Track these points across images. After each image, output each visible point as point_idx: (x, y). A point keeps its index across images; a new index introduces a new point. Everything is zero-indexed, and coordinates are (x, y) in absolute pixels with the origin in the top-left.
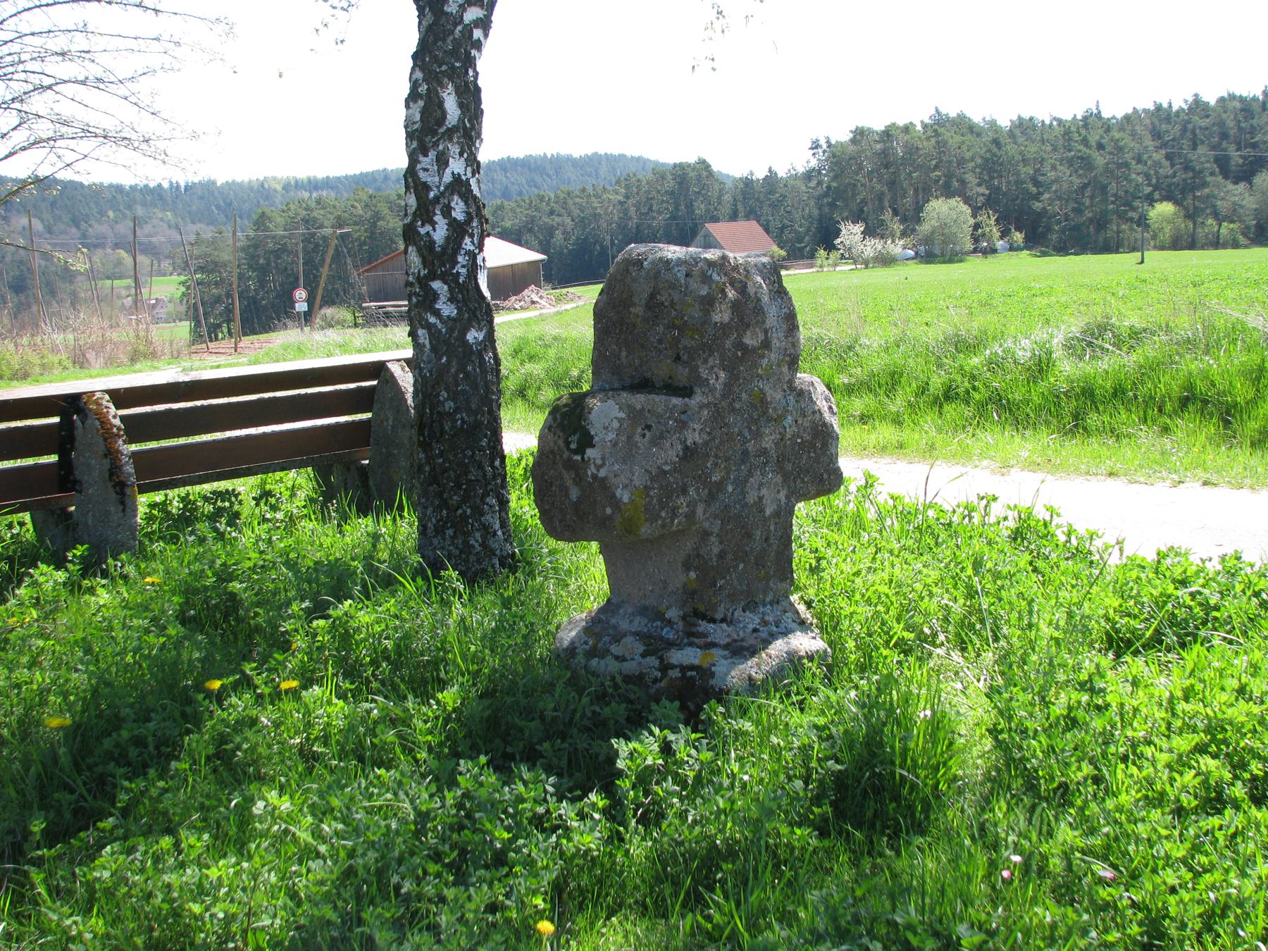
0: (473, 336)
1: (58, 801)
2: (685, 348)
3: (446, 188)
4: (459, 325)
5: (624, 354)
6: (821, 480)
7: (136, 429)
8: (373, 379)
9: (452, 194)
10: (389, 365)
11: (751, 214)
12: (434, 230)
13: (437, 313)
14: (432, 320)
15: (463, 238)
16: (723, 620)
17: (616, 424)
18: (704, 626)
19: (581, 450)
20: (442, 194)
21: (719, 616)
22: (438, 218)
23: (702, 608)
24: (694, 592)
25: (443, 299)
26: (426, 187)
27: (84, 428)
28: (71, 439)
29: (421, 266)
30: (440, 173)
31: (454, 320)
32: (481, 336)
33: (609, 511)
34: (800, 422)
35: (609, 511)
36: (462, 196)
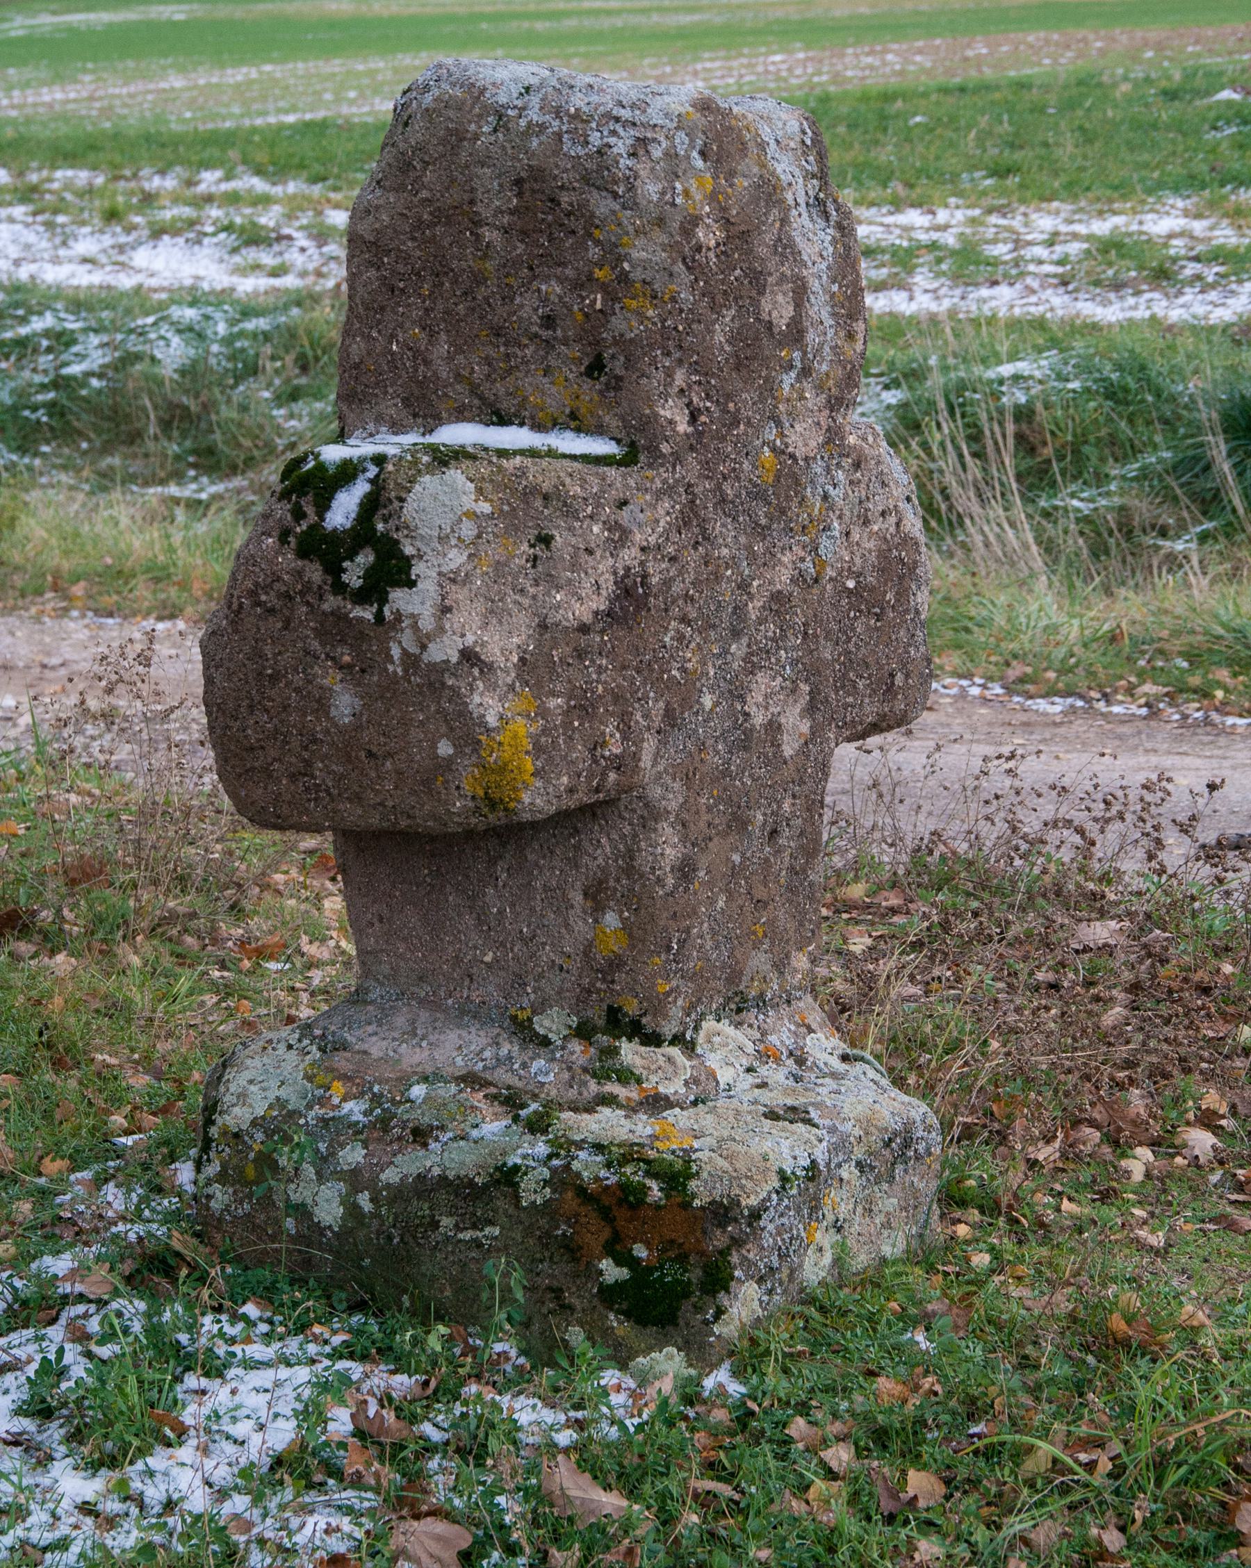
1: (691, 1365)
2: (619, 341)
6: (890, 688)
16: (677, 1040)
17: (468, 530)
18: (630, 1053)
19: (375, 589)
23: (632, 1008)
24: (616, 963)
33: (445, 749)
34: (855, 536)
35: (445, 749)
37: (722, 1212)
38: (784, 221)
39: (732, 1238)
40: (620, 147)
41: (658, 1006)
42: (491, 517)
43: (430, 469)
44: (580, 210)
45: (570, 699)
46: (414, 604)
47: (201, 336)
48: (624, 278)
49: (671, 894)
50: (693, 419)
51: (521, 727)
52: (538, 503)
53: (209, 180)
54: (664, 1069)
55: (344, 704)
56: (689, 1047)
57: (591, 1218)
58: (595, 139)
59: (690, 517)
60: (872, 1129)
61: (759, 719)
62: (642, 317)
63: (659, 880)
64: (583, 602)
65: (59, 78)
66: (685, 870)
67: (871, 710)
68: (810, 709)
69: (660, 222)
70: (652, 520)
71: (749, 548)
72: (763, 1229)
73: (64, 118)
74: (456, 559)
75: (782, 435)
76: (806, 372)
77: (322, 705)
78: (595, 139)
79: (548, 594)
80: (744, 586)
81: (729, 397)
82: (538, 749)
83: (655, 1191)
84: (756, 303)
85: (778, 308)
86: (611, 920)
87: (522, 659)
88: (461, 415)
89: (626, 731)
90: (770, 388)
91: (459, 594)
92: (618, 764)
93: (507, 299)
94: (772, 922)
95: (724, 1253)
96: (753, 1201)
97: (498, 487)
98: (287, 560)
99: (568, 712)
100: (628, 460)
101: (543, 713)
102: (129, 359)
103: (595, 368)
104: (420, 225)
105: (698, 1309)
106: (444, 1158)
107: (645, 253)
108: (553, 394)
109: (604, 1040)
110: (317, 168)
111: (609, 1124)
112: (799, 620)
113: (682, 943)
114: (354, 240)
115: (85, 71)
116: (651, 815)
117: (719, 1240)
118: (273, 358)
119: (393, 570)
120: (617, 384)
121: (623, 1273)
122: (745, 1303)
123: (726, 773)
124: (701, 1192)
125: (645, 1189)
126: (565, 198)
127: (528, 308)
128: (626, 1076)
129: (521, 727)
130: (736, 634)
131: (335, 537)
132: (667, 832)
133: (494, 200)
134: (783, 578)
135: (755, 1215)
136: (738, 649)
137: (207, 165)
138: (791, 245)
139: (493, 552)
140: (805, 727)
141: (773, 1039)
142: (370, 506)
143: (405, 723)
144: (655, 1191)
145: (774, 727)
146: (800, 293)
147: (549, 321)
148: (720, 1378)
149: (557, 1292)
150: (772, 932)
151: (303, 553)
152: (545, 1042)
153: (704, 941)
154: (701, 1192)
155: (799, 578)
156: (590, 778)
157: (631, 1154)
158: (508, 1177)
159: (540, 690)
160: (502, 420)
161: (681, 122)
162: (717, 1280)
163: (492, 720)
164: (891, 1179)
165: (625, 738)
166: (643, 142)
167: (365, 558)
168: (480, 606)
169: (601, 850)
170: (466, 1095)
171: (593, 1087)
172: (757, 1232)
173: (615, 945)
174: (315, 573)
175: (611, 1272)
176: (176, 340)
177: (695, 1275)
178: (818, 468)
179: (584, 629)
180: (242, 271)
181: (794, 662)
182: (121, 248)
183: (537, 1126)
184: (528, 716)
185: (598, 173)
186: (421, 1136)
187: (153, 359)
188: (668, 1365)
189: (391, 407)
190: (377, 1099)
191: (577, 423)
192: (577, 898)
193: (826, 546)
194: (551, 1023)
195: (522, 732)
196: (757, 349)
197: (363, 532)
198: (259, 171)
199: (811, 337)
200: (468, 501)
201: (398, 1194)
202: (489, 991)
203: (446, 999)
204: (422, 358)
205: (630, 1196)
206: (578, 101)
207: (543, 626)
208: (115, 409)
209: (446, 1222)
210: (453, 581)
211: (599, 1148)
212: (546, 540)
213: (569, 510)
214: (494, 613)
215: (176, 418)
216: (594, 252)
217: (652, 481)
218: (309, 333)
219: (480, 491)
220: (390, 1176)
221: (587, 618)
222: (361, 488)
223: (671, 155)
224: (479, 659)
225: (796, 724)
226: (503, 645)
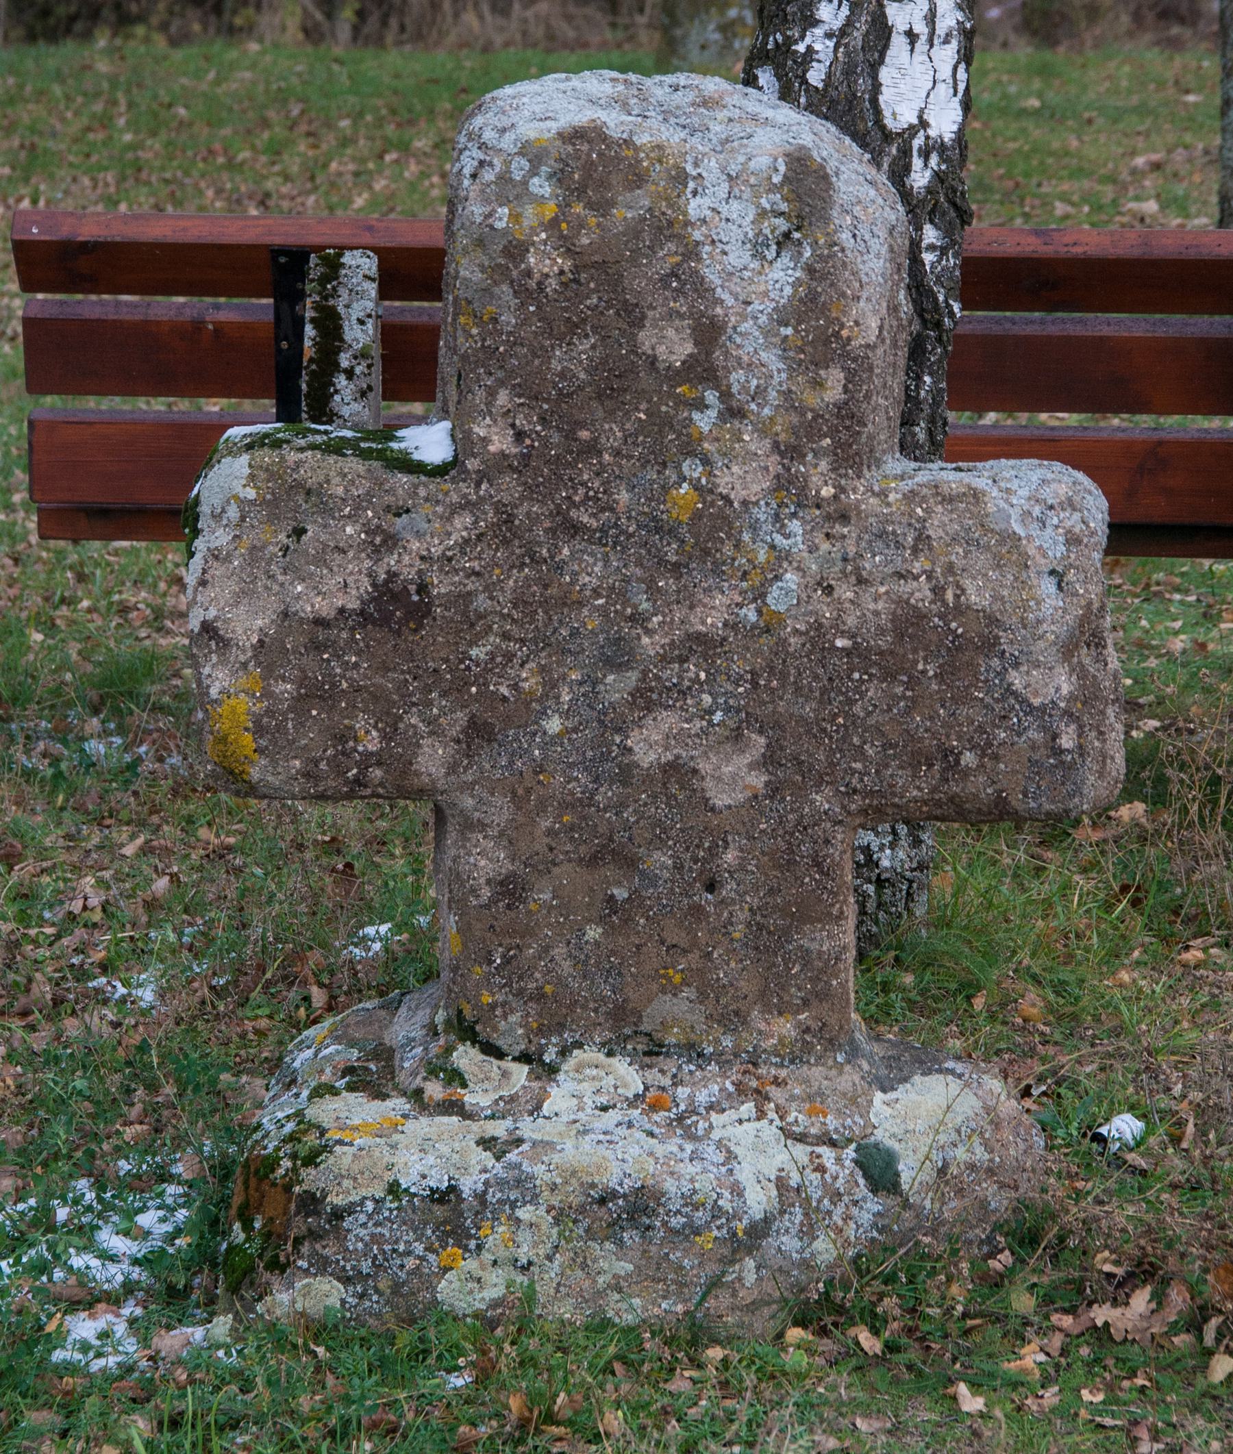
16: (524, 1058)
17: (233, 513)
39: (309, 1230)
42: (252, 503)
45: (300, 687)
49: (487, 906)
50: (519, 436)
51: (243, 705)
52: (300, 499)
60: (574, 1181)
63: (473, 891)
64: (337, 589)
68: (769, 761)
72: (349, 1231)
75: (710, 474)
79: (291, 583)
81: (582, 425)
87: (260, 641)
91: (218, 570)
101: (267, 694)
113: (507, 961)
128: (456, 1077)
135: (338, 1214)
136: (617, 686)
140: (758, 780)
146: (709, 332)
159: (269, 672)
172: (341, 1236)
178: (761, 514)
179: (320, 622)
184: (254, 695)
195: (242, 709)
207: (285, 614)
210: (216, 558)
212: (299, 532)
217: (446, 494)
219: (252, 477)
223: (504, 179)
224: (216, 633)
226: (248, 625)
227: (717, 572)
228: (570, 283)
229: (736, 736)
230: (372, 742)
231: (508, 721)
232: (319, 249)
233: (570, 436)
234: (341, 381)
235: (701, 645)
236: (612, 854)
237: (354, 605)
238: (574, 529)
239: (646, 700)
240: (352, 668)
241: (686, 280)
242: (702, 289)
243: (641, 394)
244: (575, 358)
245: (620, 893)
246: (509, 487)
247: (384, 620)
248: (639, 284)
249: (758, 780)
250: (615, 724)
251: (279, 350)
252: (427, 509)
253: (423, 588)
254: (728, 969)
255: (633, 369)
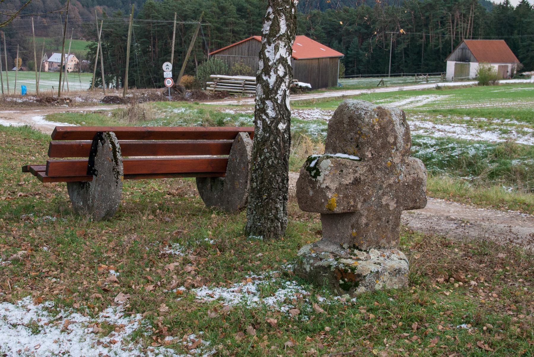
0: (282, 126)
2: (361, 142)
3: (277, 61)
4: (276, 121)
5: (338, 142)
7: (126, 150)
8: (232, 139)
9: (279, 64)
10: (241, 134)
11: (499, 35)
12: (270, 78)
13: (267, 115)
14: (264, 117)
15: (281, 83)
16: (365, 251)
17: (329, 168)
18: (356, 251)
19: (315, 177)
20: (275, 63)
21: (363, 249)
22: (272, 73)
23: (357, 245)
24: (355, 238)
25: (270, 109)
26: (268, 60)
27: (103, 147)
28: (96, 151)
29: (262, 93)
30: (275, 54)
31: (274, 118)
32: (284, 126)
33: (323, 201)
35: (323, 201)
36: (283, 65)
37: (359, 275)
38: (394, 126)
40: (363, 113)
41: (361, 245)
43: (325, 159)
44: (357, 123)
46: (320, 178)
47: (478, 149)
48: (362, 133)
50: (372, 155)
51: (335, 198)
53: (507, 121)
54: (362, 255)
55: (311, 193)
56: (368, 253)
57: (340, 274)
58: (360, 112)
59: (370, 170)
61: (384, 203)
62: (364, 139)
64: (348, 180)
65: (513, 100)
66: (367, 225)
67: (411, 205)
68: (397, 203)
69: (368, 125)
70: (362, 170)
71: (384, 176)
73: (510, 108)
74: (327, 172)
76: (397, 150)
77: (308, 193)
78: (360, 112)
80: (383, 182)
81: (380, 152)
82: (337, 202)
83: (350, 271)
84: (386, 139)
85: (391, 140)
86: (354, 231)
88: (340, 152)
89: (355, 201)
90: (389, 152)
91: (327, 178)
92: (353, 206)
93: (346, 135)
94: (386, 235)
95: (358, 281)
96: (365, 274)
97: (335, 162)
98: (305, 171)
99: (343, 197)
100: (360, 160)
101: (339, 197)
102: (464, 153)
103: (357, 146)
104: (336, 123)
105: (353, 289)
106: (323, 263)
107: (365, 129)
108: (351, 150)
109: (352, 249)
110: (528, 119)
111: (349, 261)
112: (395, 189)
113: (366, 236)
114: (329, 125)
115: (520, 99)
116: (361, 215)
117: (358, 279)
118: (490, 154)
119: (318, 173)
120: (360, 149)
121: (343, 282)
122: (361, 290)
123: (376, 210)
124: (356, 272)
125: (348, 270)
126: (355, 120)
127: (349, 137)
128: (355, 255)
129: (335, 198)
130: (380, 189)
131: (311, 168)
132: (363, 218)
133: (346, 120)
134: (391, 182)
135: (365, 277)
136: (381, 192)
137: (507, 118)
138: (395, 130)
139: (333, 172)
140: (395, 205)
141: (385, 254)
142: (316, 164)
143: (318, 196)
144: (350, 271)
145: (387, 205)
146: (396, 138)
147: (351, 139)
148: (354, 300)
149: (334, 284)
150: (386, 237)
151: (307, 170)
152: (344, 248)
153: (370, 235)
154: (356, 272)
155: (395, 182)
156: (347, 208)
157: (348, 265)
158: (330, 266)
159: (338, 193)
160: (345, 153)
161: (373, 110)
162: (357, 285)
163: (330, 197)
164: (396, 276)
165: (354, 202)
166: (366, 113)
167: (315, 171)
168: (330, 180)
169: (354, 220)
170: (330, 254)
171: (349, 256)
172: (365, 280)
173: (355, 235)
174: (308, 173)
175: (341, 282)
176: (473, 150)
177: (353, 284)
178: (399, 165)
179: (347, 185)
180: (500, 138)
181: (393, 195)
182: (479, 133)
183: (337, 260)
185: (359, 117)
186: (321, 259)
187: (468, 153)
188: (347, 296)
189: (331, 150)
190: (317, 254)
191: (354, 155)
192: (350, 227)
193: (400, 178)
194: (345, 246)
196: (385, 145)
197: (315, 168)
198: (517, 120)
199: (398, 145)
200: (330, 164)
201: (316, 268)
202: (338, 240)
203: (331, 240)
204: (335, 143)
205: (345, 271)
206: (358, 106)
207: (340, 184)
208: (459, 162)
209: (322, 272)
211: (344, 264)
212: (342, 171)
213: (346, 167)
214: (332, 181)
215: (470, 164)
216: (358, 129)
218: (498, 150)
220: (316, 265)
221: (348, 183)
222: (316, 161)
223: (371, 115)
225: (393, 205)
226: (333, 186)
227: (393, 174)
228: (380, 131)
229: (393, 199)
230: (352, 204)
231: (368, 199)
232: (105, 132)
233: (379, 154)
234: (117, 153)
235: (390, 185)
236: (379, 219)
237: (351, 182)
238: (378, 168)
239: (383, 194)
240: (350, 192)
241: (393, 130)
242: (395, 131)
243: (388, 148)
244: (379, 142)
245: (379, 224)
246: (371, 162)
247: (355, 184)
248: (388, 131)
249: (395, 205)
250: (380, 198)
251: (91, 149)
252: (360, 166)
253: (360, 179)
254: (389, 235)
255: (386, 144)
